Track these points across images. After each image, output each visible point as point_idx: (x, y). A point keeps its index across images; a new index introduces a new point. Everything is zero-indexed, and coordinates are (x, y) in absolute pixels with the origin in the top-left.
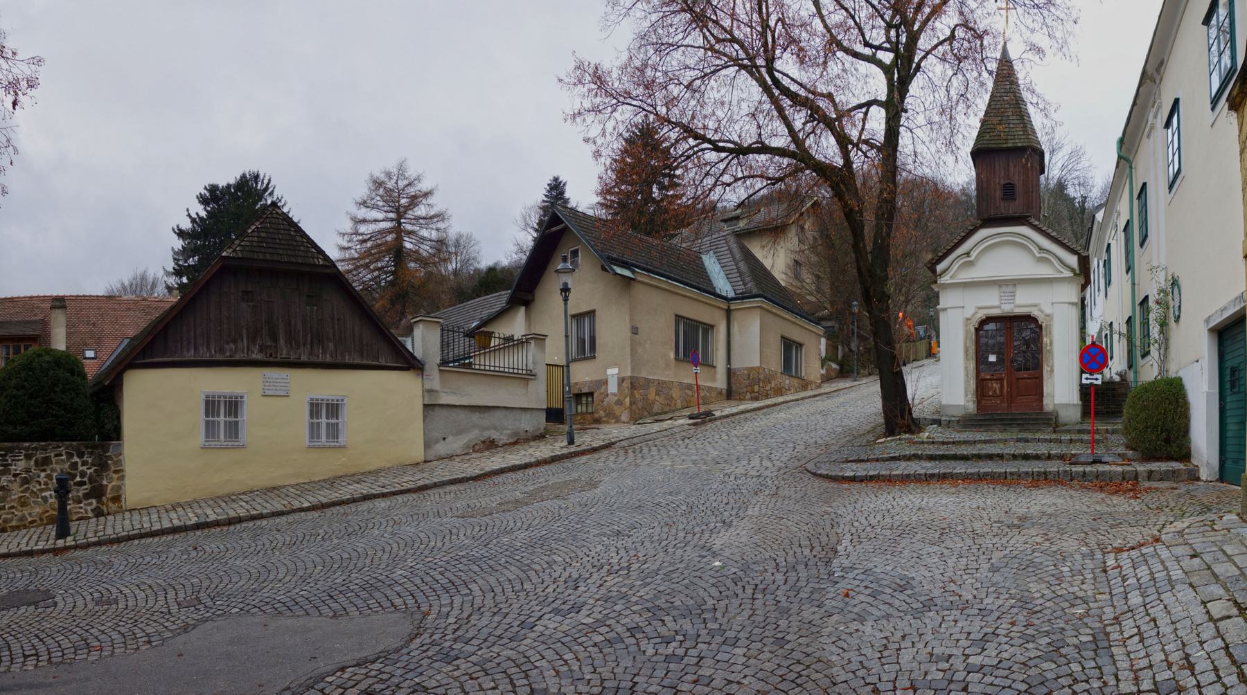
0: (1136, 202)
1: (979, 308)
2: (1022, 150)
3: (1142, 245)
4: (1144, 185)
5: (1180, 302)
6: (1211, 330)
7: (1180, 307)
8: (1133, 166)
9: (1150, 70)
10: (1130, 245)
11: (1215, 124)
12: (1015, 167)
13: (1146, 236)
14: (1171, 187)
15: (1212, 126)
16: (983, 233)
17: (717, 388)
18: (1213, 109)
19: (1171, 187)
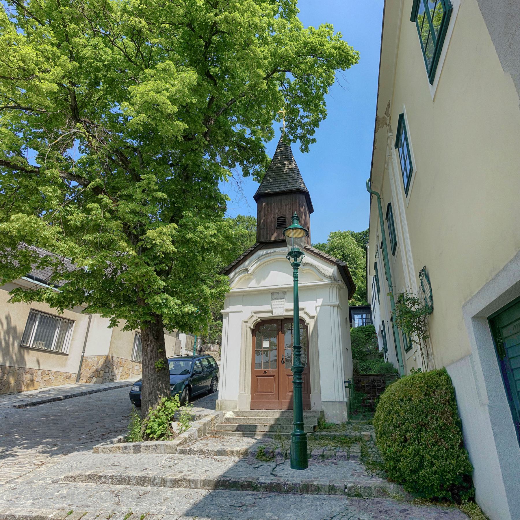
0: (385, 222)
1: (255, 313)
2: (291, 192)
3: (394, 253)
4: (389, 205)
5: (431, 291)
6: (476, 318)
7: (431, 297)
8: (381, 198)
9: (381, 115)
10: (385, 255)
11: (436, 100)
12: (286, 205)
13: (396, 244)
14: (407, 191)
15: (434, 101)
16: (261, 252)
17: (64, 373)
18: (432, 82)
19: (407, 191)
